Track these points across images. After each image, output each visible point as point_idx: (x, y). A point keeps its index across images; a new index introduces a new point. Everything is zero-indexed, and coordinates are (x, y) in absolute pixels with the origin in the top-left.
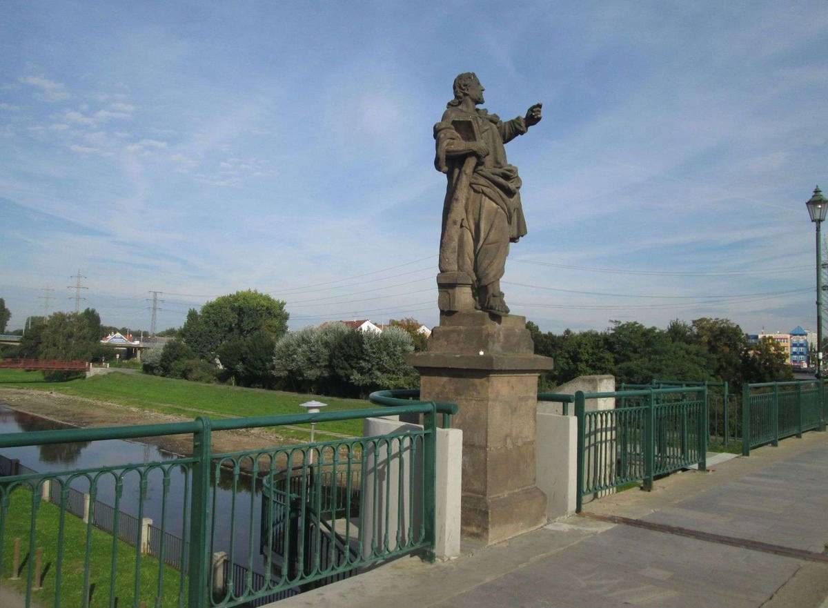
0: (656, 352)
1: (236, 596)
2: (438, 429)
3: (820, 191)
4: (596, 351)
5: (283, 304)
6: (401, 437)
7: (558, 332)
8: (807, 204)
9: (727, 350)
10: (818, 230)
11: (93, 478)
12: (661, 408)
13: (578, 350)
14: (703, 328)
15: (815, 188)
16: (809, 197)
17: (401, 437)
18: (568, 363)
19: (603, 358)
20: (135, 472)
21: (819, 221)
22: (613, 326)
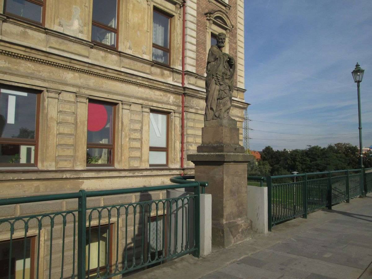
0: (327, 157)
1: (137, 265)
2: (200, 194)
3: (359, 66)
4: (303, 157)
5: (285, 150)
6: (183, 199)
7: (281, 149)
8: (352, 73)
9: (352, 156)
10: (358, 86)
11: (109, 209)
12: (318, 181)
13: (295, 157)
14: (339, 147)
15: (357, 64)
16: (353, 68)
17: (183, 199)
18: (291, 162)
19: (306, 160)
20: (35, 219)
21: (359, 82)
22: (309, 147)
